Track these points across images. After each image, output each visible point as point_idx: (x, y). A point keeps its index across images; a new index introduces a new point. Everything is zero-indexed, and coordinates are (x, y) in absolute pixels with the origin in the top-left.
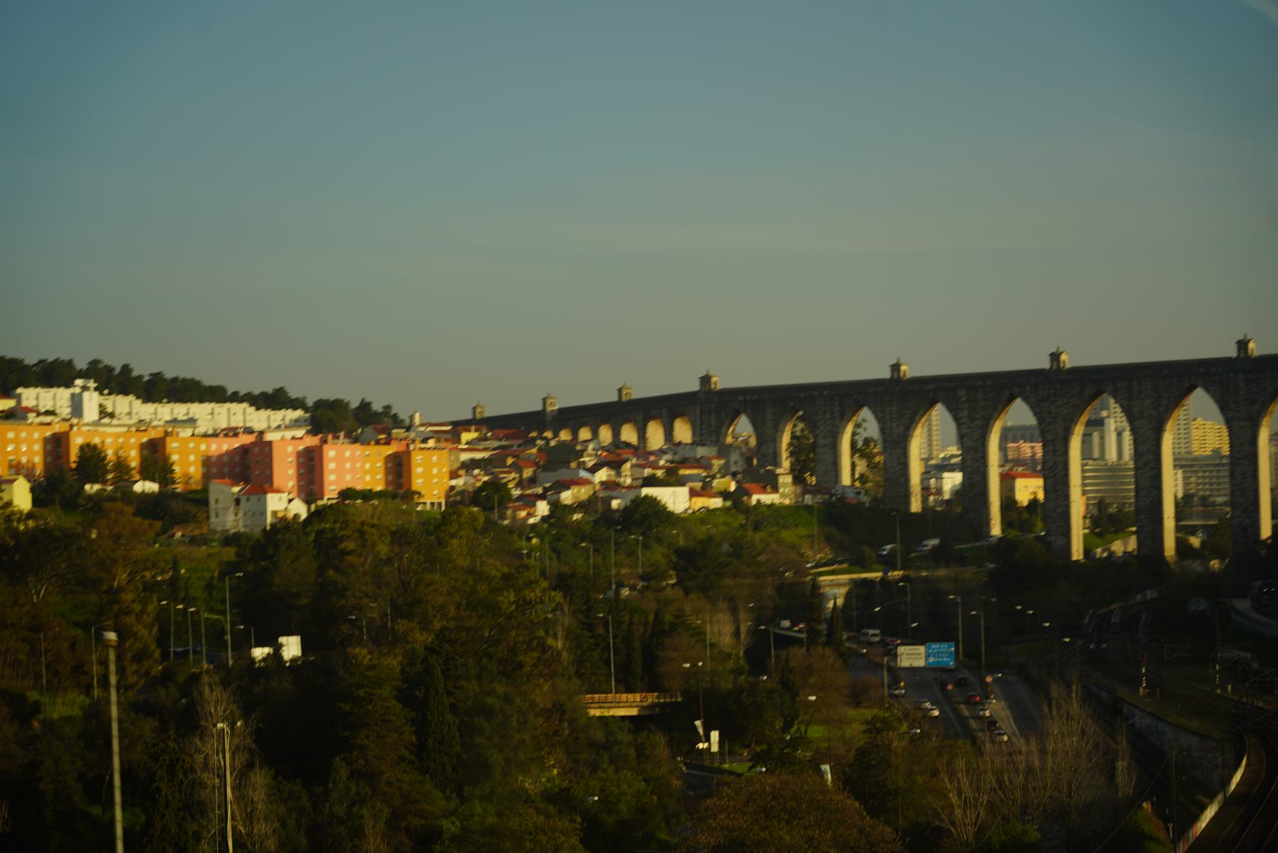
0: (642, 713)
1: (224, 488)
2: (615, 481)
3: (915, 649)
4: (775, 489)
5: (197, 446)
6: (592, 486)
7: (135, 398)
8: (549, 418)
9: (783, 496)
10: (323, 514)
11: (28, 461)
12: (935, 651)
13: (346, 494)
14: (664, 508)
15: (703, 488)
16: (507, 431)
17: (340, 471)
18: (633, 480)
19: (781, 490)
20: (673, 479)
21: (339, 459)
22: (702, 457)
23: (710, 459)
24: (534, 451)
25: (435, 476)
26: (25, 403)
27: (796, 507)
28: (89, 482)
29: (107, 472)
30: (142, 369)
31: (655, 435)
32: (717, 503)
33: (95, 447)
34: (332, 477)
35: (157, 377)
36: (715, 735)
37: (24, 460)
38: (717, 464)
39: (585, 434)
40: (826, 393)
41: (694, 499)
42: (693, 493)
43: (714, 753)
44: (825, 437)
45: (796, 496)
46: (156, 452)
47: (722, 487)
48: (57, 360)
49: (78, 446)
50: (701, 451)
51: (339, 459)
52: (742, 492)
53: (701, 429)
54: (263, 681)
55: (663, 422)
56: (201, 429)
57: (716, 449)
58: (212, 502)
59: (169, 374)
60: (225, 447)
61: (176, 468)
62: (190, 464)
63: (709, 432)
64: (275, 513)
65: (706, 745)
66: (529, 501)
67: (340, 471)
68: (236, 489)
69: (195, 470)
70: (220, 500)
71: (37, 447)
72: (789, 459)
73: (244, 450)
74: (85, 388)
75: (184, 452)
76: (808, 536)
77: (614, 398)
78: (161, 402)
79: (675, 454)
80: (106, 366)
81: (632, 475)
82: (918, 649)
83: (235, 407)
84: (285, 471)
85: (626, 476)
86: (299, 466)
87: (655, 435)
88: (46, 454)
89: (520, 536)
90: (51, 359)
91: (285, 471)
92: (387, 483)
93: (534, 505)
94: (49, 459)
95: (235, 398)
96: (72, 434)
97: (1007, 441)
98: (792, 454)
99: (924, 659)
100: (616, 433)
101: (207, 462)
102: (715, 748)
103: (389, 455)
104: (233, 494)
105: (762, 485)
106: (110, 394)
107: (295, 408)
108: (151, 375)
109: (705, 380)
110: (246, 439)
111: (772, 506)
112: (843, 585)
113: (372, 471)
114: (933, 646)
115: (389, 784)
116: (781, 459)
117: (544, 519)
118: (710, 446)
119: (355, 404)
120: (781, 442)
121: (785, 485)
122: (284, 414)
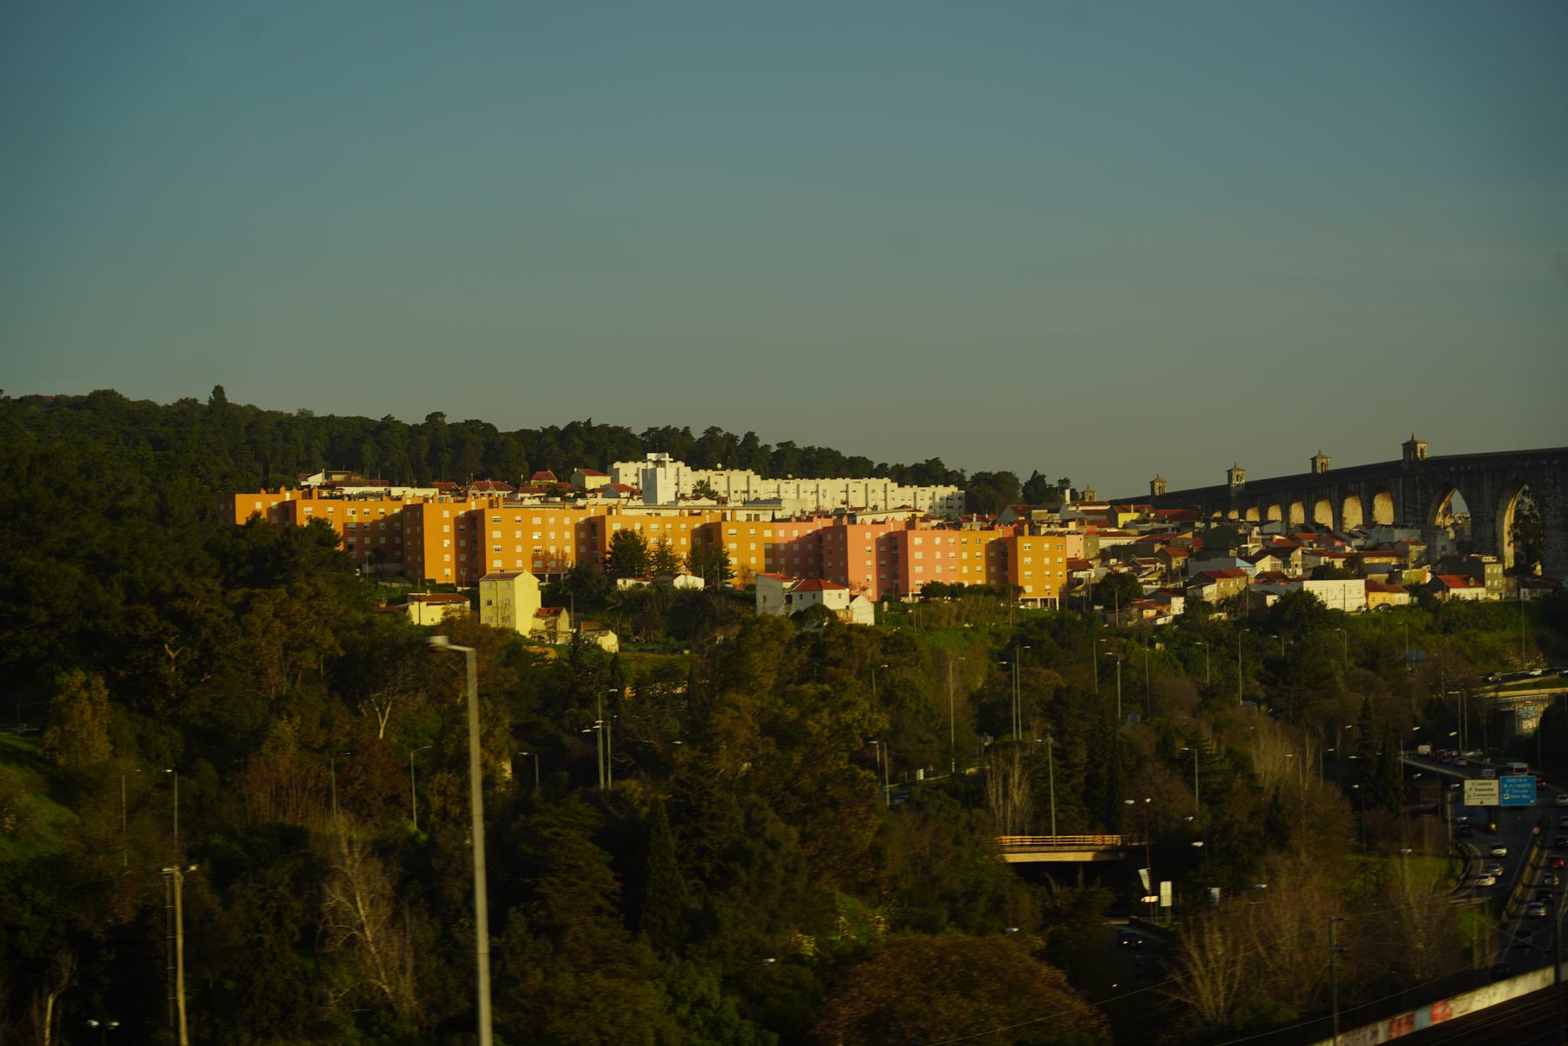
0: (1097, 859)
1: (774, 583)
2: (1280, 572)
3: (1486, 784)
4: (1481, 582)
5: (759, 533)
6: (1245, 578)
7: (753, 473)
8: (1233, 495)
9: (1491, 590)
10: (804, 616)
11: (558, 552)
12: (1511, 786)
13: (931, 590)
14: (1322, 605)
15: (1389, 581)
16: (1173, 512)
17: (928, 562)
18: (1304, 571)
19: (1488, 583)
20: (1354, 569)
21: (928, 548)
22: (1399, 541)
23: (1406, 544)
24: (1189, 535)
25: (1048, 567)
26: (623, 481)
27: (1506, 603)
28: (620, 577)
29: (649, 564)
30: (770, 439)
31: (1353, 514)
32: (1403, 598)
33: (633, 533)
34: (919, 569)
35: (787, 447)
36: (1166, 888)
37: (552, 550)
38: (1415, 551)
39: (1252, 515)
40: (1555, 462)
41: (1372, 595)
42: (1371, 587)
43: (1165, 907)
44: (1555, 516)
45: (1508, 589)
46: (711, 540)
47: (1414, 579)
48: (668, 427)
49: (613, 533)
50: (1399, 535)
51: (928, 548)
52: (1437, 585)
53: (1404, 507)
54: (522, 817)
55: (1360, 499)
56: (787, 513)
57: (1419, 531)
58: (760, 600)
59: (800, 444)
60: (796, 534)
61: (733, 561)
62: (752, 554)
63: (1414, 513)
64: (570, 626)
65: (1154, 899)
66: (1162, 598)
67: (928, 562)
68: (787, 585)
69: (756, 562)
70: (768, 598)
71: (568, 535)
72: (1512, 545)
73: (818, 536)
74: (658, 463)
75: (744, 540)
76: (1514, 640)
77: (1307, 469)
78: (785, 478)
79: (1368, 538)
80: (728, 434)
81: (1303, 565)
82: (1491, 784)
83: (874, 483)
84: (863, 562)
85: (1296, 565)
86: (879, 556)
87: (1353, 514)
88: (579, 542)
89: (1140, 641)
90: (661, 427)
91: (863, 562)
92: (989, 576)
93: (1169, 602)
94: (583, 549)
95: (879, 472)
96: (608, 518)
97: (821, 575)
98: (1516, 538)
99: (1497, 796)
100: (1309, 513)
101: (772, 552)
102: (1166, 901)
103: (992, 543)
104: (784, 589)
105: (1463, 576)
106: (724, 469)
107: (947, 485)
108: (780, 445)
109: (1410, 447)
110: (819, 524)
111: (1474, 603)
112: (1542, 701)
113: (970, 562)
114: (1508, 780)
115: (577, 939)
116: (1503, 542)
117: (1177, 619)
118: (1412, 528)
119: (1024, 478)
120: (1503, 524)
121: (1493, 577)
122: (932, 491)
